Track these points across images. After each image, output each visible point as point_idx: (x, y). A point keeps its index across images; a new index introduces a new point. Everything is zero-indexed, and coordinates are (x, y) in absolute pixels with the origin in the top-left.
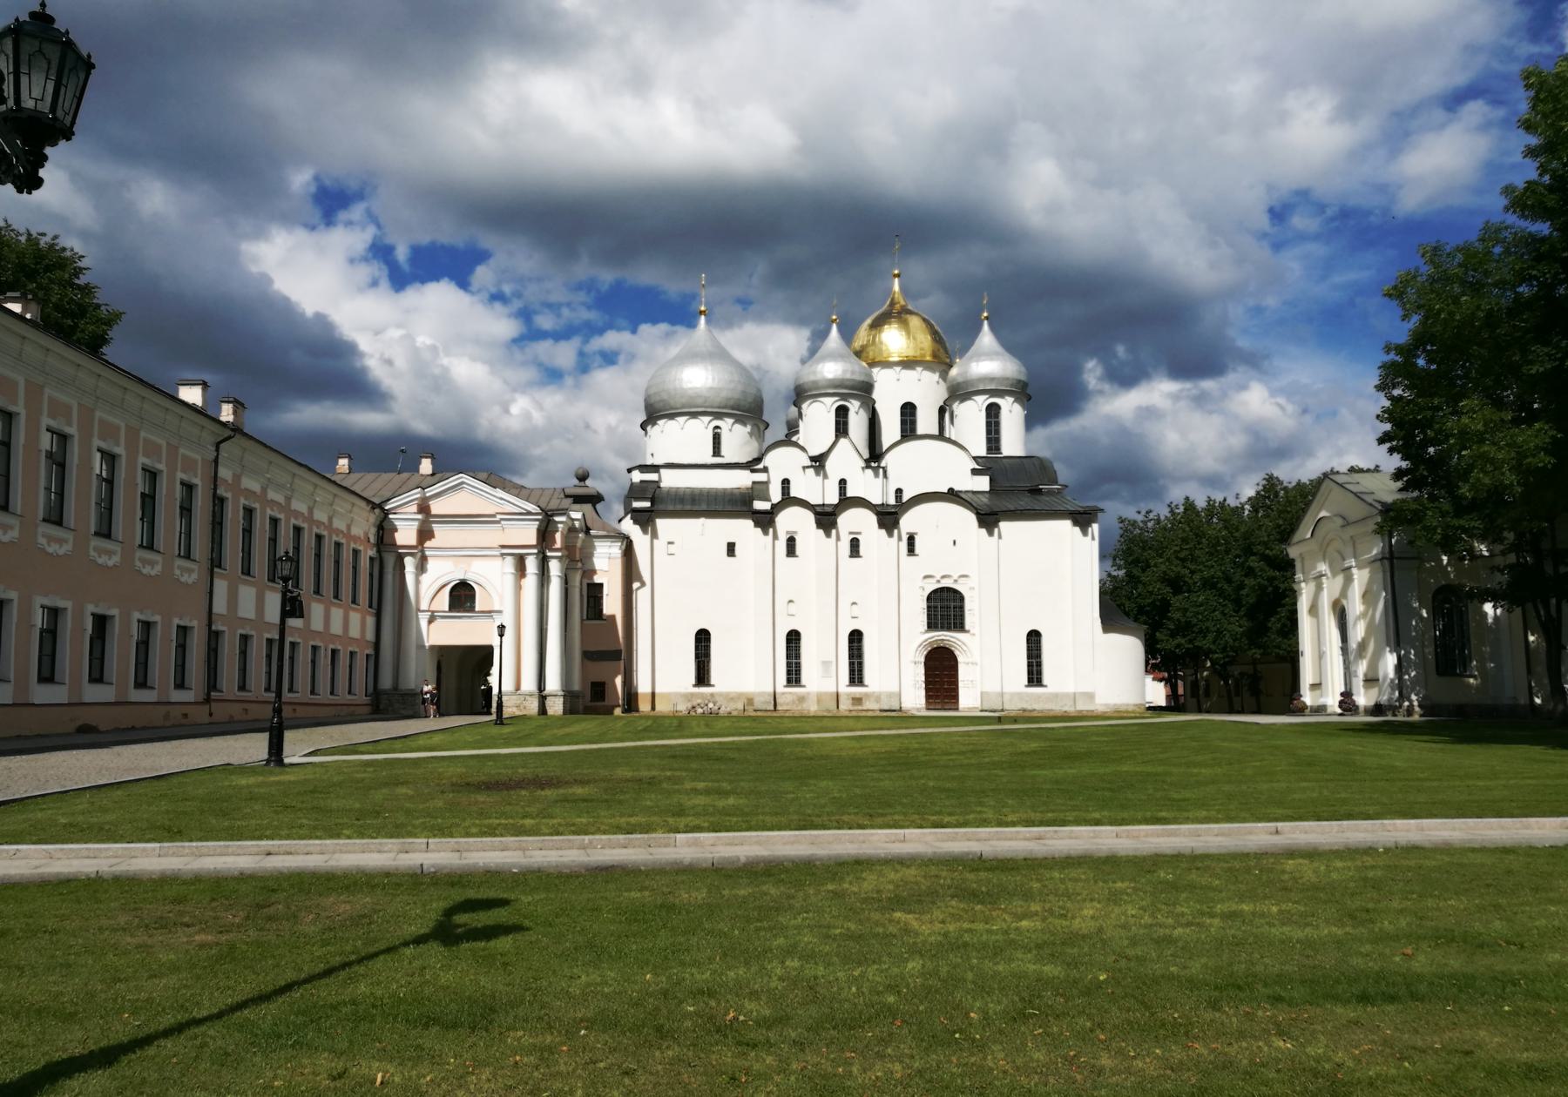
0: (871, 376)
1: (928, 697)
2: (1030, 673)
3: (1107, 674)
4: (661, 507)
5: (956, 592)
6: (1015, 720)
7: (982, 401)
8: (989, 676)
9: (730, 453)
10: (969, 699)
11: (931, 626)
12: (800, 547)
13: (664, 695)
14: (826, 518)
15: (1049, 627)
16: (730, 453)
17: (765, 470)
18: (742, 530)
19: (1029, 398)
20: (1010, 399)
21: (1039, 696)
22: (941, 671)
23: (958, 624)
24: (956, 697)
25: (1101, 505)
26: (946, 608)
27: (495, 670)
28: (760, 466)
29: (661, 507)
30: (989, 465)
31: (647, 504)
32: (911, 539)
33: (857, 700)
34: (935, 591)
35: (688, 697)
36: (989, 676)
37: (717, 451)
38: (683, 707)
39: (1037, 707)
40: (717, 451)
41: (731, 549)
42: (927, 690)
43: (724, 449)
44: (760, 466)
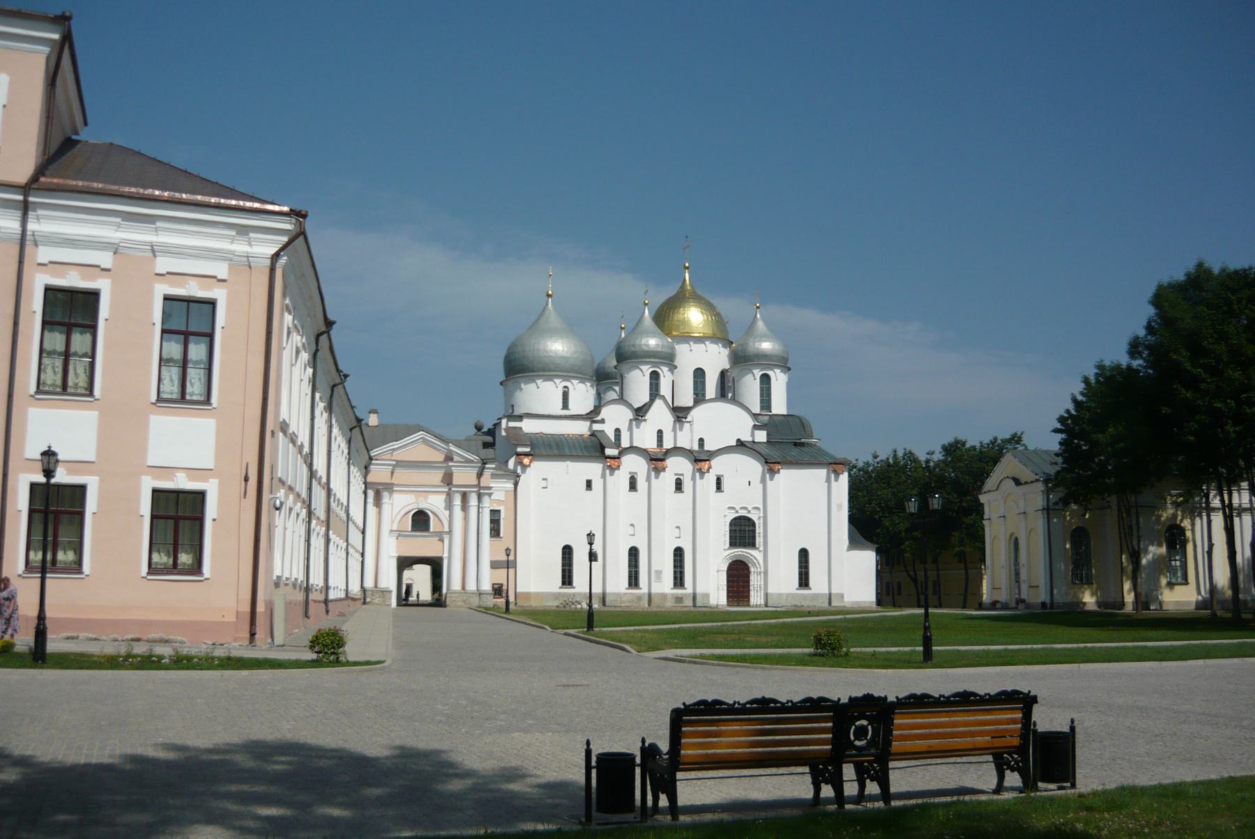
0: (673, 348)
1: (728, 597)
2: (800, 579)
3: (853, 577)
4: (537, 451)
5: (749, 519)
6: (809, 614)
7: (647, 369)
8: (775, 581)
9: (574, 408)
10: (756, 598)
11: (733, 544)
12: (726, 484)
13: (63, 623)
14: (657, 460)
15: (816, 549)
16: (574, 408)
17: (603, 421)
18: (593, 469)
19: (789, 369)
20: (777, 371)
21: (805, 596)
22: (738, 576)
23: (752, 544)
24: (748, 597)
25: (33, 450)
26: (743, 532)
27: (1190, 547)
28: (599, 418)
29: (537, 451)
30: (766, 421)
31: (528, 450)
32: (719, 482)
33: (679, 599)
34: (735, 519)
35: (556, 596)
36: (775, 581)
37: (565, 405)
38: (553, 604)
39: (805, 603)
40: (565, 405)
41: (589, 484)
42: (728, 592)
43: (571, 405)
44: (599, 418)
